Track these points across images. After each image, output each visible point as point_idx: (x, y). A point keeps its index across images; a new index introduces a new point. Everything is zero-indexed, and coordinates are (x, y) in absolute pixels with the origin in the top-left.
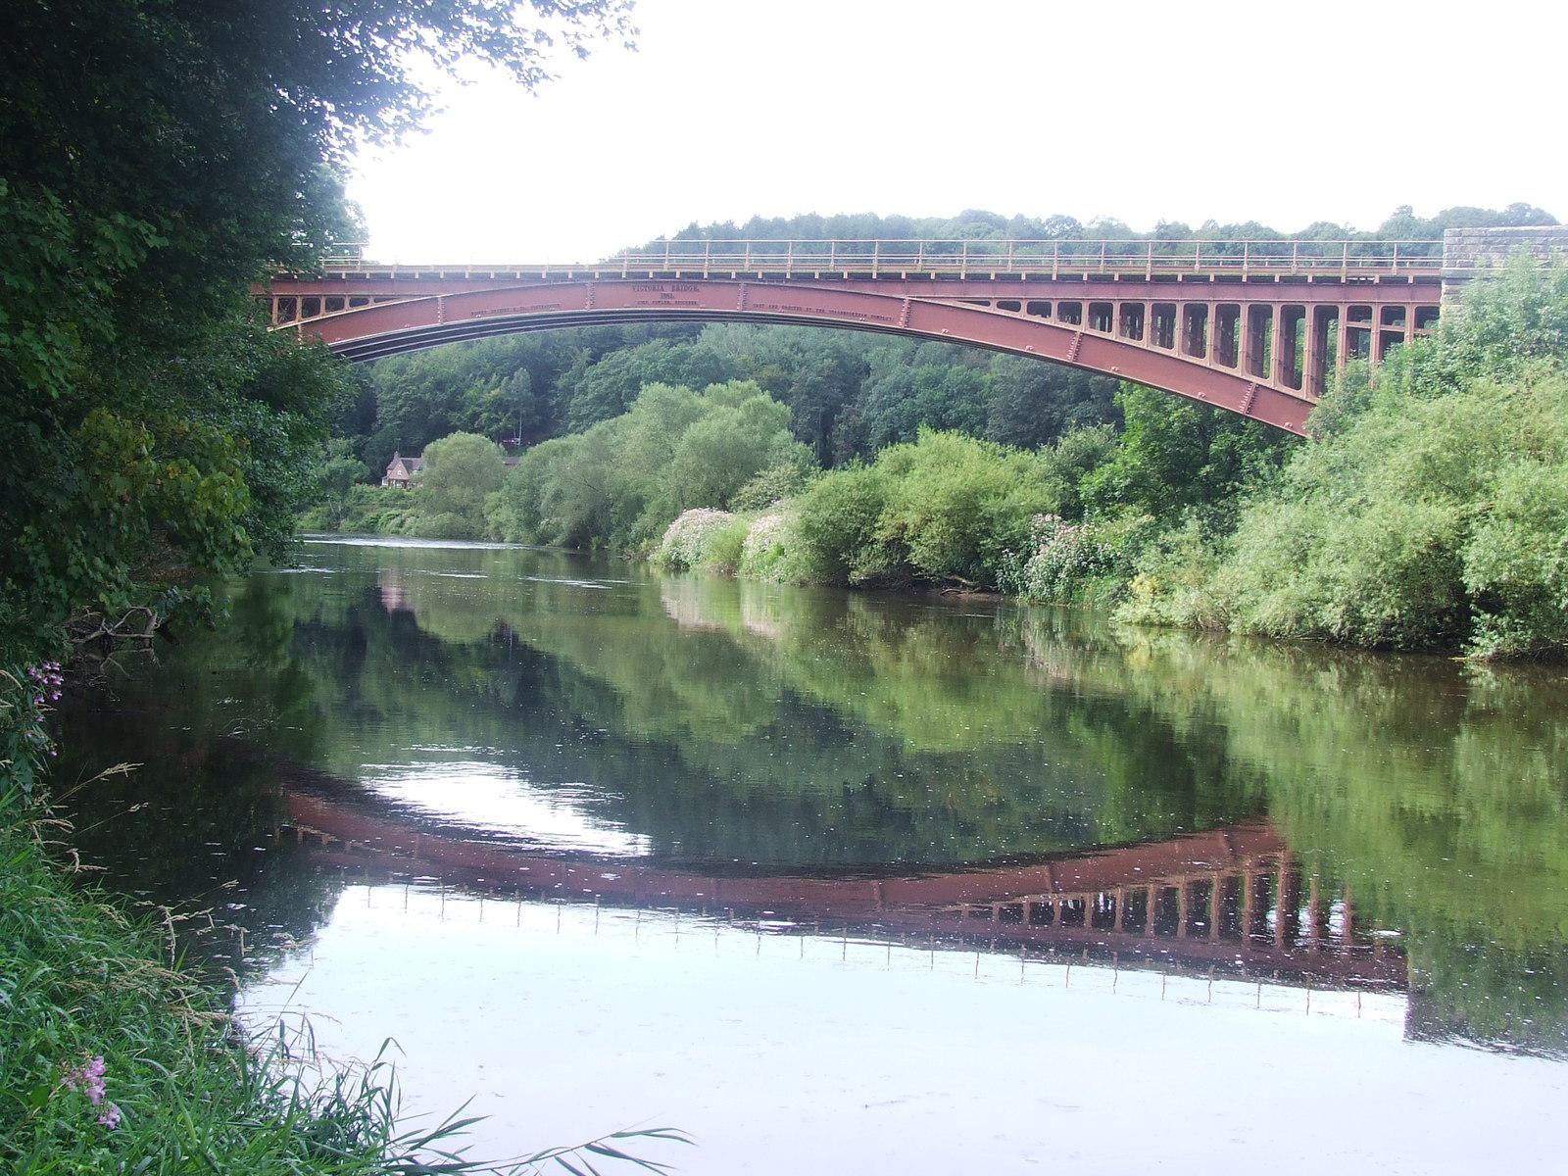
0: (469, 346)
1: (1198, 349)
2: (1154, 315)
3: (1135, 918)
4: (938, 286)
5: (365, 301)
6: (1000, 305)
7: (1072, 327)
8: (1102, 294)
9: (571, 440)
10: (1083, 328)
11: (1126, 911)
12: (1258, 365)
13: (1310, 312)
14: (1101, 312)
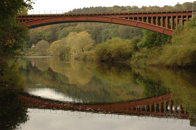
0: (43, 27)
1: (150, 23)
2: (144, 19)
3: (148, 110)
4: (116, 16)
5: (29, 20)
6: (125, 18)
7: (136, 21)
8: (140, 16)
9: (59, 41)
10: (138, 21)
11: (147, 109)
12: (164, 25)
13: (172, 17)
14: (140, 18)
